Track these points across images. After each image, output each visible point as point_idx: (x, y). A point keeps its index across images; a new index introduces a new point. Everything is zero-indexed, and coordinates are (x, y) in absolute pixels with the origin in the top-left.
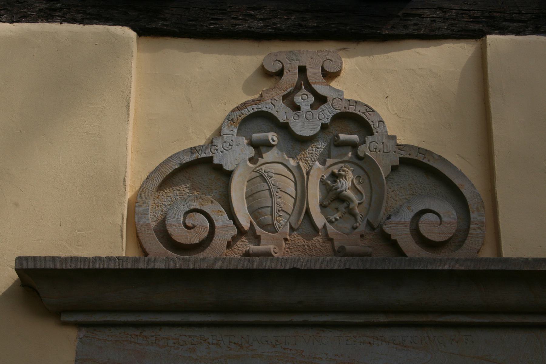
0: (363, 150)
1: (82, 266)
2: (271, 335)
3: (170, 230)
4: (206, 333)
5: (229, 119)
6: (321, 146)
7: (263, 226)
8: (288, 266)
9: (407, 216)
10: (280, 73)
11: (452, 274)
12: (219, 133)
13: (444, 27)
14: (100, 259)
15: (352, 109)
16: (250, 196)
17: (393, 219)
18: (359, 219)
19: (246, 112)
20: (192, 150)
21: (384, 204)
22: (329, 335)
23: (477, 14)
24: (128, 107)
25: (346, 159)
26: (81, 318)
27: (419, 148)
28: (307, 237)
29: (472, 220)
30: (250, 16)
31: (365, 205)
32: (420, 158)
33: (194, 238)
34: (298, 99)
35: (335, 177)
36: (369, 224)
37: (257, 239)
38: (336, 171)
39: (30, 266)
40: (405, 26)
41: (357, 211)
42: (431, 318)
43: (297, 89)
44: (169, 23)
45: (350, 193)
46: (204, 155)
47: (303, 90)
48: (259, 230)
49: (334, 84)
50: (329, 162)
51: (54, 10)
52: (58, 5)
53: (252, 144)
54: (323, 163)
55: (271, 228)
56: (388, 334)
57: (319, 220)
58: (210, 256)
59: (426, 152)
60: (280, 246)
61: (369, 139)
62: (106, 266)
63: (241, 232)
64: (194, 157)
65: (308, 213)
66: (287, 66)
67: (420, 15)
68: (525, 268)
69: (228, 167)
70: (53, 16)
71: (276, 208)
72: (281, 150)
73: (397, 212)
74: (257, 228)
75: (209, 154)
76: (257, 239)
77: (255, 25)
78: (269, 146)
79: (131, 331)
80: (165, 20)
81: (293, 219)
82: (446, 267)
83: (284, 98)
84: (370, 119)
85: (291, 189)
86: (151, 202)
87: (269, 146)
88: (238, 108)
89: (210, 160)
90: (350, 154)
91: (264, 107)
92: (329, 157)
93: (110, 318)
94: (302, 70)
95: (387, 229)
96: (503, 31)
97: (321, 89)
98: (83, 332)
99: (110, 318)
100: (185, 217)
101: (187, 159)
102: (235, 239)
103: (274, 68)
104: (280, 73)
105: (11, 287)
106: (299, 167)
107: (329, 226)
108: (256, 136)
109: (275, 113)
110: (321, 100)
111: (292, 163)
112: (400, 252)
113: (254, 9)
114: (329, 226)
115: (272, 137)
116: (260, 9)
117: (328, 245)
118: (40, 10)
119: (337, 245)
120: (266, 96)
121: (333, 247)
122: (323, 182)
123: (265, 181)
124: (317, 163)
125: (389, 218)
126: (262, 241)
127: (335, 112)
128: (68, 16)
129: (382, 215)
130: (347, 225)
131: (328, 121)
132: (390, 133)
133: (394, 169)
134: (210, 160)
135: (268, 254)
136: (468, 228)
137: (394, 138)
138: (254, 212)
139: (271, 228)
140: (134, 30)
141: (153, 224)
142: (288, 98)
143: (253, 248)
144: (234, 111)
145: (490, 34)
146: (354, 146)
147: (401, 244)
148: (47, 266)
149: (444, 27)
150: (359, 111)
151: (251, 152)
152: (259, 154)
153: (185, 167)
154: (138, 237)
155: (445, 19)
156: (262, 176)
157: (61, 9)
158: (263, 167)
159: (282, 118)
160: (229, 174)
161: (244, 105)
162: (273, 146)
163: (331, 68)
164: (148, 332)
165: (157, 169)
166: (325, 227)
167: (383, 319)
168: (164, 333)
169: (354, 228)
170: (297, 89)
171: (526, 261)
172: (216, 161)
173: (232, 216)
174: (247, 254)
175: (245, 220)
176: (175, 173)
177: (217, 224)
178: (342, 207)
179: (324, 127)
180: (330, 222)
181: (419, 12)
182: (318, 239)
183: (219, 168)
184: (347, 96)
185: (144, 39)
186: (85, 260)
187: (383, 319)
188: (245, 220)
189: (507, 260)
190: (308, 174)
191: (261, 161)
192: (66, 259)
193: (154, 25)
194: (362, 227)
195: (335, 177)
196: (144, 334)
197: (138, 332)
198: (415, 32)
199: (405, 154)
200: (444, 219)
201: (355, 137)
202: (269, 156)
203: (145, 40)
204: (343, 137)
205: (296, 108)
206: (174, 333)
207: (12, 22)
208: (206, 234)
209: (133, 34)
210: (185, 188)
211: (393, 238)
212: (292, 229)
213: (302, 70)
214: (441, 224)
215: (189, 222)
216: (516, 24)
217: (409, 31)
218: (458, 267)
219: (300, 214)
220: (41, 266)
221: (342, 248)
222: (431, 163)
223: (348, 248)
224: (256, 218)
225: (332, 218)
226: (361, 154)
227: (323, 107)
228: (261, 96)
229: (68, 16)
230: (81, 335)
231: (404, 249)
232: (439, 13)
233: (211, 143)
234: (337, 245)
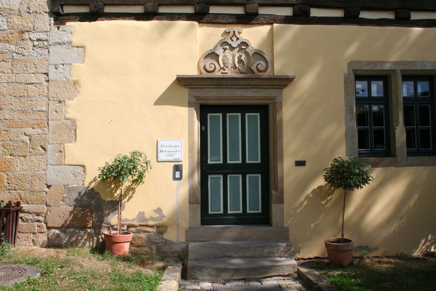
0: (247, 50)
2: (227, 90)
4: (214, 89)
5: (219, 43)
6: (238, 49)
7: (226, 67)
10: (229, 32)
12: (216, 46)
13: (265, 22)
14: (193, 75)
16: (223, 60)
17: (253, 65)
20: (211, 50)
21: (251, 62)
22: (239, 90)
23: (272, 19)
24: (197, 40)
25: (243, 52)
26: (189, 87)
27: (258, 50)
28: (235, 69)
30: (223, 19)
31: (247, 62)
32: (259, 52)
33: (211, 69)
34: (233, 39)
35: (241, 56)
37: (224, 70)
38: (241, 55)
39: (179, 77)
41: (245, 63)
42: (259, 87)
43: (233, 36)
44: (205, 21)
45: (244, 60)
48: (225, 68)
49: (241, 35)
51: (180, 18)
52: (181, 17)
53: (223, 49)
54: (238, 53)
55: (227, 67)
56: (251, 90)
57: (237, 65)
58: (338, 274)
59: (260, 51)
60: (229, 71)
61: (248, 48)
62: (195, 77)
63: (221, 68)
64: (211, 52)
65: (235, 64)
67: (259, 19)
69: (218, 54)
70: (180, 19)
71: (228, 63)
73: (253, 64)
74: (224, 67)
76: (224, 70)
77: (224, 21)
78: (226, 49)
79: (199, 89)
80: (204, 20)
81: (232, 65)
82: (263, 77)
84: (248, 43)
85: (232, 59)
87: (226, 49)
88: (220, 41)
90: (244, 51)
91: (226, 40)
93: (195, 87)
94: (234, 32)
95: (251, 68)
96: (277, 23)
97: (238, 36)
99: (195, 87)
100: (210, 65)
101: (210, 52)
102: (220, 70)
103: (228, 31)
104: (229, 32)
106: (233, 54)
108: (224, 47)
109: (228, 42)
110: (238, 39)
111: (232, 53)
112: (254, 73)
113: (223, 17)
115: (228, 47)
116: (225, 17)
117: (239, 71)
119: (241, 71)
121: (240, 71)
122: (238, 57)
123: (226, 57)
125: (252, 65)
127: (241, 41)
128: (183, 19)
129: (250, 64)
130: (243, 67)
131: (239, 44)
133: (253, 54)
134: (214, 52)
135: (227, 73)
136: (268, 68)
137: (253, 47)
138: (224, 64)
139: (227, 67)
140: (198, 22)
141: (203, 66)
142: (231, 39)
143: (224, 72)
144: (219, 41)
145: (274, 23)
146: (245, 49)
148: (183, 77)
149: (265, 22)
150: (246, 41)
151: (223, 50)
152: (225, 51)
153: (209, 54)
155: (265, 20)
156: (225, 56)
157: (181, 17)
158: (226, 54)
159: (230, 43)
160: (219, 56)
162: (227, 49)
163: (240, 31)
164: (203, 89)
165: (203, 54)
166: (238, 67)
167: (250, 87)
168: (206, 89)
169: (244, 67)
170: (233, 36)
172: (216, 53)
173: (219, 65)
174: (222, 73)
175: (222, 65)
178: (242, 63)
179: (238, 45)
180: (240, 66)
181: (259, 18)
182: (237, 69)
183: (216, 54)
187: (250, 87)
188: (222, 65)
189: (275, 76)
190: (235, 55)
192: (186, 75)
193: (202, 21)
195: (241, 56)
200: (263, 66)
201: (245, 47)
202: (227, 51)
203: (200, 24)
204: (243, 47)
205: (233, 41)
206: (208, 89)
207: (171, 21)
209: (197, 23)
210: (209, 58)
212: (232, 67)
213: (234, 32)
216: (280, 21)
217: (257, 23)
218: (265, 77)
220: (181, 77)
221: (242, 72)
222: (261, 53)
223: (243, 72)
224: (224, 65)
225: (240, 65)
226: (246, 51)
227: (238, 40)
228: (225, 38)
229: (183, 19)
230: (189, 90)
231: (255, 72)
232: (264, 18)
233: (214, 48)
234: (241, 71)
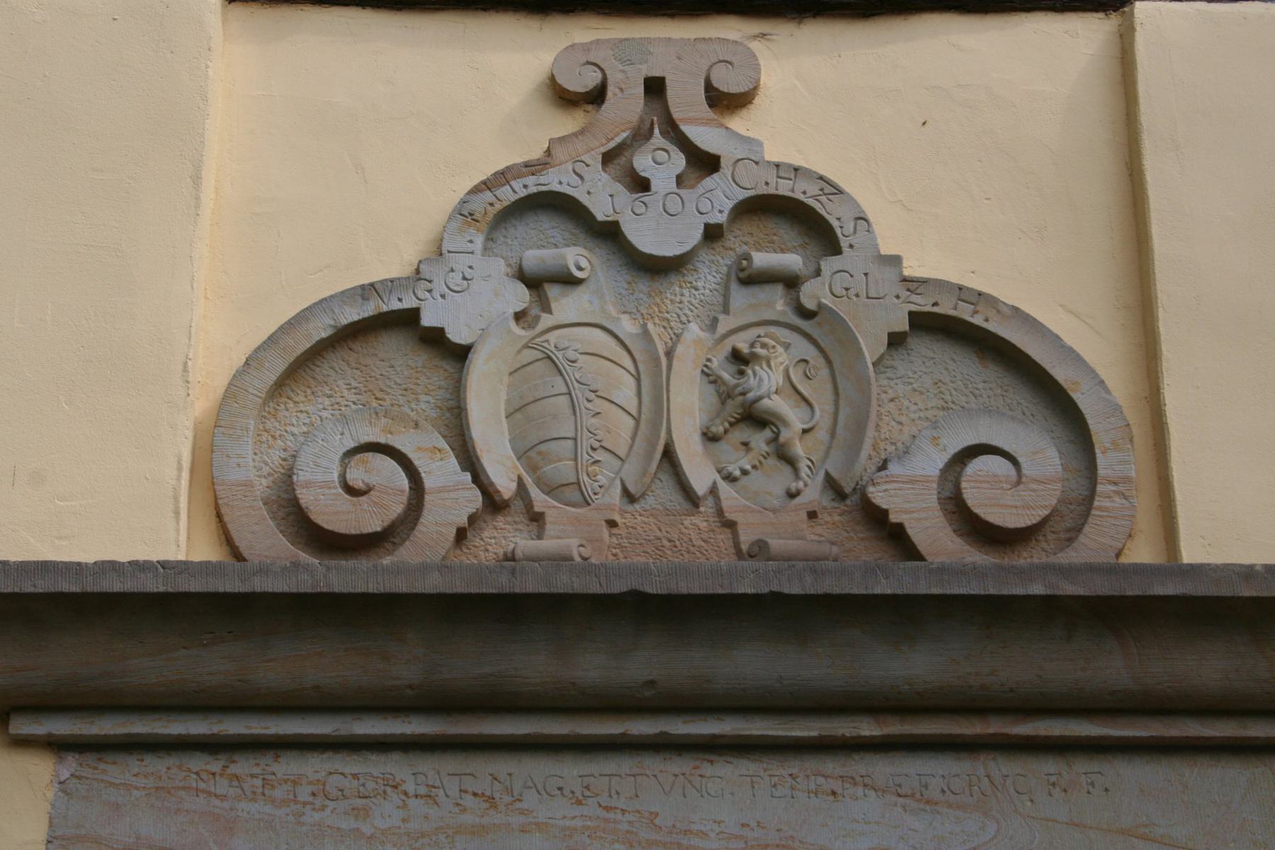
5: (463, 214)
8: (618, 587)
9: (931, 462)
10: (597, 96)
15: (784, 188)
16: (517, 411)
19: (508, 195)
24: (197, 180)
29: (1101, 471)
32: (964, 312)
34: (643, 162)
43: (641, 135)
46: (395, 305)
47: (658, 139)
48: (539, 499)
56: (882, 768)
63: (493, 504)
69: (458, 335)
75: (409, 303)
82: (1037, 589)
84: (831, 211)
85: (626, 392)
88: (486, 185)
94: (655, 88)
97: (705, 137)
98: (71, 764)
104: (597, 96)
108: (535, 258)
110: (704, 163)
114: (724, 488)
126: (550, 529)
127: (742, 195)
132: (885, 251)
134: (409, 319)
146: (791, 282)
147: (916, 533)
150: (803, 191)
151: (519, 296)
158: (552, 337)
159: (601, 212)
160: (461, 354)
163: (728, 82)
164: (244, 766)
167: (867, 728)
168: (288, 766)
170: (641, 135)
172: (427, 320)
173: (470, 461)
177: (428, 483)
183: (435, 340)
184: (772, 154)
190: (669, 354)
197: (215, 765)
199: (923, 304)
200: (1026, 470)
201: (792, 261)
205: (641, 185)
206: (313, 767)
211: (893, 518)
213: (655, 88)
214: (1019, 482)
226: (810, 304)
227: (709, 182)
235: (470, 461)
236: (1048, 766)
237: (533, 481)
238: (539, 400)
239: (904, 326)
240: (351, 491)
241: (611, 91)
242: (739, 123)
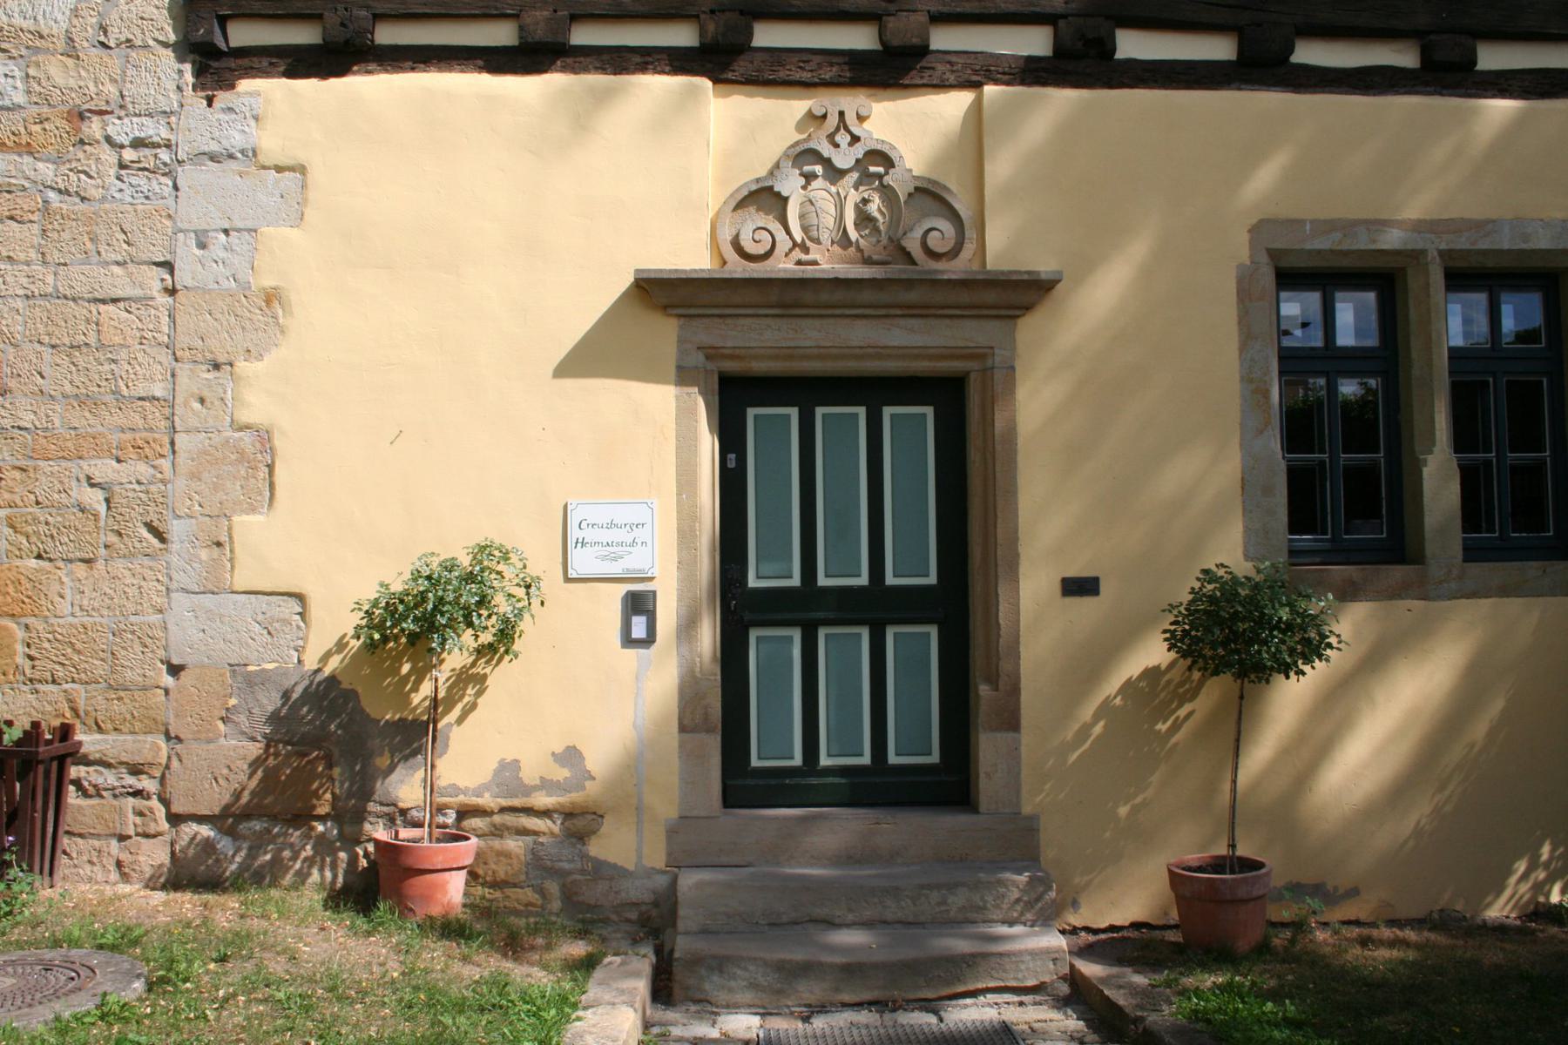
0: (887, 180)
1: (684, 276)
2: (817, 322)
3: (742, 243)
4: (769, 321)
5: (786, 155)
6: (855, 175)
7: (812, 240)
8: (831, 276)
9: (918, 233)
10: (824, 116)
11: (949, 281)
12: (777, 166)
13: (952, 79)
14: (695, 271)
15: (879, 147)
16: (802, 217)
17: (908, 235)
18: (883, 235)
19: (799, 149)
20: (758, 180)
21: (902, 223)
22: (859, 323)
23: (978, 68)
24: (708, 145)
29: (967, 236)
30: (800, 68)
32: (930, 187)
33: (760, 250)
34: (838, 138)
35: (865, 201)
36: (890, 238)
37: (806, 250)
40: (922, 77)
41: (882, 228)
43: (838, 129)
45: (876, 214)
46: (767, 184)
47: (842, 130)
48: (808, 243)
50: (861, 188)
51: (647, 63)
53: (802, 174)
55: (818, 241)
56: (902, 322)
57: (853, 234)
63: (795, 244)
66: (830, 111)
67: (933, 68)
68: (1002, 278)
69: (785, 194)
70: (647, 69)
72: (825, 179)
73: (911, 230)
74: (807, 241)
75: (770, 184)
76: (806, 250)
77: (806, 76)
80: (734, 71)
82: (946, 277)
83: (828, 136)
84: (893, 155)
85: (832, 210)
86: (728, 221)
88: (792, 146)
89: (771, 188)
90: (877, 183)
91: (813, 145)
92: (861, 185)
93: (701, 311)
94: (841, 114)
96: (996, 82)
97: (856, 131)
98: (682, 320)
99: (701, 311)
101: (754, 187)
102: (791, 250)
103: (819, 112)
104: (824, 116)
105: (628, 289)
106: (838, 193)
107: (861, 240)
108: (807, 168)
110: (855, 139)
111: (833, 189)
112: (913, 263)
113: (804, 62)
114: (861, 240)
115: (818, 169)
116: (808, 61)
117: (859, 254)
118: (637, 64)
119: (866, 255)
120: (813, 136)
122: (856, 205)
123: (812, 204)
124: (852, 190)
125: (905, 234)
126: (811, 251)
127: (867, 149)
128: (659, 69)
129: (901, 232)
130: (874, 240)
132: (908, 167)
133: (910, 195)
134: (771, 188)
135: (815, 263)
137: (911, 170)
138: (805, 229)
139: (818, 241)
142: (831, 138)
143: (804, 257)
145: (986, 84)
146: (880, 177)
147: (913, 254)
149: (952, 79)
150: (885, 149)
151: (802, 181)
152: (808, 182)
153: (752, 194)
154: (718, 248)
155: (953, 71)
156: (810, 201)
157: (652, 63)
158: (812, 193)
159: (826, 154)
160: (786, 199)
161: (797, 143)
163: (863, 112)
164: (729, 321)
165: (732, 195)
167: (899, 312)
168: (742, 321)
170: (838, 129)
171: (1002, 273)
172: (776, 189)
173: (788, 232)
175: (798, 235)
176: (745, 198)
177: (777, 239)
179: (858, 161)
180: (861, 236)
182: (852, 249)
183: (778, 194)
184: (875, 137)
185: (717, 86)
186: (685, 271)
187: (899, 312)
188: (798, 235)
190: (845, 198)
191: (810, 188)
192: (670, 271)
194: (884, 240)
195: (865, 201)
196: (726, 322)
197: (721, 321)
198: (929, 83)
199: (919, 184)
200: (946, 236)
201: (881, 170)
202: (818, 183)
203: (721, 87)
204: (872, 169)
205: (837, 146)
206: (748, 321)
207: (615, 74)
208: (769, 247)
209: (709, 84)
210: (752, 209)
211: (908, 250)
212: (833, 242)
213: (841, 114)
214: (943, 239)
215: (757, 238)
217: (925, 81)
219: (839, 231)
220: (653, 276)
221: (870, 257)
222: (938, 191)
225: (862, 233)
226: (885, 184)
227: (857, 145)
228: (810, 135)
229: (659, 69)
232: (948, 66)
233: (771, 173)
234: (866, 255)
235: (788, 232)
236: (947, 321)
237: (264, 670)
238: (1230, 6)
239: (913, 191)
240: (755, 241)
241: (829, 116)
242: (866, 125)
